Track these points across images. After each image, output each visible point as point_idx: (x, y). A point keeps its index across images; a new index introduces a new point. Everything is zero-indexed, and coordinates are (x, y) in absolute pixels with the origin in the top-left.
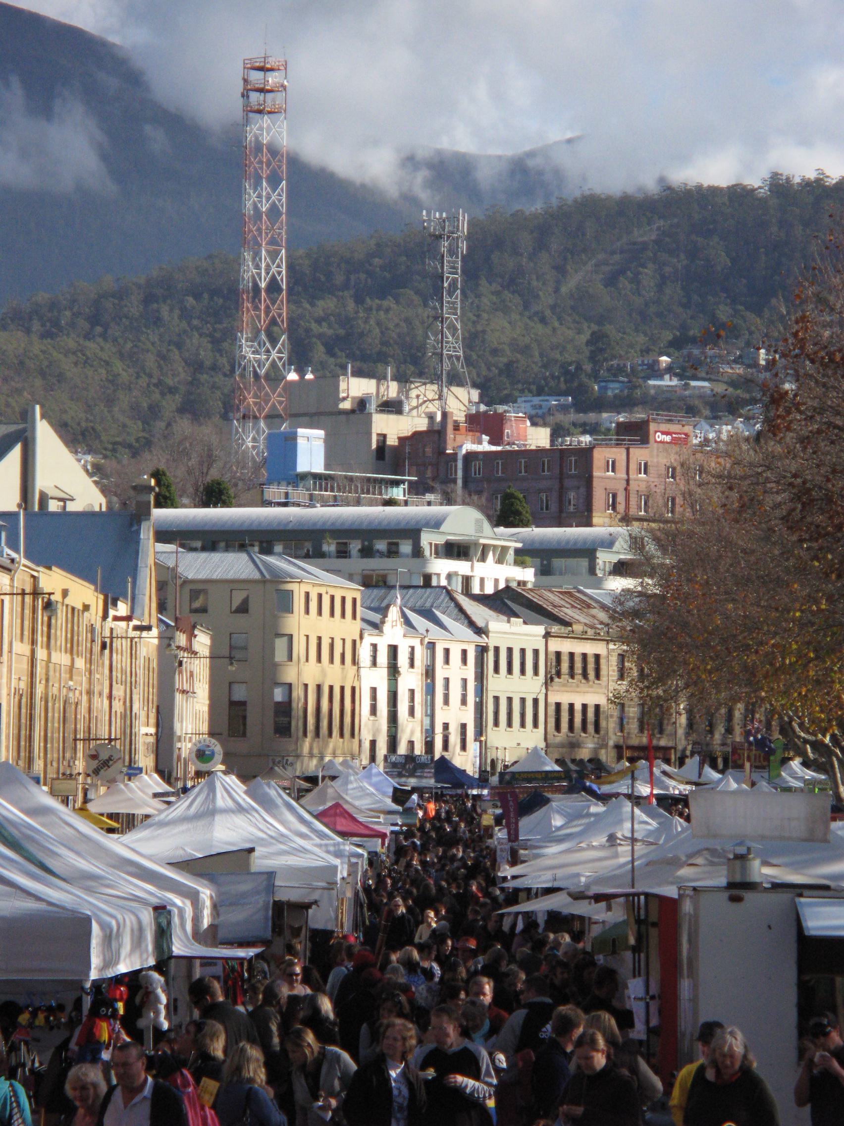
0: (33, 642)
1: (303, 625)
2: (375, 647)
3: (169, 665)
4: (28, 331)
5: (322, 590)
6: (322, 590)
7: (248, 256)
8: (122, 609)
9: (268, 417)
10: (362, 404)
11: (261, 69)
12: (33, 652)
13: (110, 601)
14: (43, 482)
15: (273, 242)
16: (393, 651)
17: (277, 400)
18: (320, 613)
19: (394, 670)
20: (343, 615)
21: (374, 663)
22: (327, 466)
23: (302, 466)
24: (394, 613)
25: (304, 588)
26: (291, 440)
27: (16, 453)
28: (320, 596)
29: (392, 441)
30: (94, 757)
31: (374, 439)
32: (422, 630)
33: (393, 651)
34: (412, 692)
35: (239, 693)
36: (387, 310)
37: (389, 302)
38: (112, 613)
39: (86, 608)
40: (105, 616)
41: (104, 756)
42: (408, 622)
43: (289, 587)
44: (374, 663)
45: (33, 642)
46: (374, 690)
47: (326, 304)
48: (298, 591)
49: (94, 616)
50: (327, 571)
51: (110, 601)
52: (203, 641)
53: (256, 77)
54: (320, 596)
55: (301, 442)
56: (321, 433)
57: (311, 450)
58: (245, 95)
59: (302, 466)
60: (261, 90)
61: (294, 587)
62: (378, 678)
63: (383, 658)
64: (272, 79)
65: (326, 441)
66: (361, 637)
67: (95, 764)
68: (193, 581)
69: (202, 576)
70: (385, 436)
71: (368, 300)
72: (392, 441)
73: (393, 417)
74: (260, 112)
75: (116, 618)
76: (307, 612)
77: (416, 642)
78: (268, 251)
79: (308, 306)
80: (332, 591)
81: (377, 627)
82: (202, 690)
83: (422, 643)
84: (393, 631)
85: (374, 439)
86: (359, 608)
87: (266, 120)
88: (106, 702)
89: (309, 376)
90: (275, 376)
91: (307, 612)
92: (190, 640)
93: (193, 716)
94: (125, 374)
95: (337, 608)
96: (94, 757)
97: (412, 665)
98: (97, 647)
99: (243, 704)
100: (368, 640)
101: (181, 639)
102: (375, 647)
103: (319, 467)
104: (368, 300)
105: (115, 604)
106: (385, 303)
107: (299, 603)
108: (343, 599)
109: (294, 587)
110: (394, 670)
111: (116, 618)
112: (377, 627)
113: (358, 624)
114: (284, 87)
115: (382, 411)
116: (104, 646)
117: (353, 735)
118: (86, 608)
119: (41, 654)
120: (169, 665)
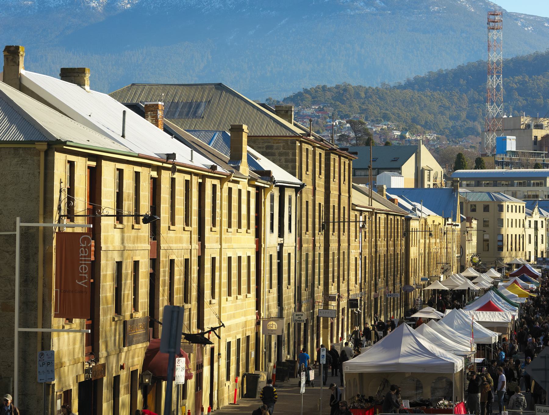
0: (425, 238)
1: (507, 216)
2: (530, 221)
3: (464, 232)
4: (413, 89)
5: (513, 204)
6: (513, 204)
7: (489, 77)
8: (450, 221)
9: (497, 130)
10: (528, 126)
12: (425, 241)
13: (446, 219)
14: (423, 165)
15: (498, 72)
16: (536, 222)
17: (500, 126)
18: (512, 212)
19: (536, 229)
21: (530, 227)
23: (508, 148)
24: (536, 210)
25: (507, 203)
26: (505, 140)
27: (413, 157)
28: (512, 206)
29: (539, 138)
30: (442, 268)
31: (533, 137)
32: (545, 215)
33: (536, 222)
34: (542, 235)
35: (486, 237)
38: (447, 223)
39: (439, 224)
40: (445, 225)
41: (445, 268)
42: (541, 213)
43: (502, 203)
44: (530, 227)
45: (425, 238)
46: (530, 235)
48: (505, 205)
49: (442, 226)
50: (486, 328)
51: (446, 219)
52: (475, 223)
53: (492, 17)
54: (512, 206)
55: (508, 141)
56: (515, 137)
57: (511, 144)
58: (488, 24)
59: (508, 148)
60: (494, 22)
61: (504, 204)
62: (531, 231)
64: (497, 18)
65: (517, 140)
66: (526, 219)
67: (443, 270)
68: (471, 202)
69: (474, 200)
71: (533, 76)
72: (539, 138)
73: (539, 130)
74: (493, 29)
75: (448, 224)
78: (496, 76)
79: (511, 78)
80: (516, 204)
81: (531, 215)
82: (474, 238)
84: (536, 216)
85: (533, 137)
86: (525, 208)
87: (495, 32)
88: (446, 250)
90: (498, 117)
91: (508, 211)
92: (470, 224)
93: (471, 248)
94: (447, 103)
95: (517, 210)
96: (442, 268)
97: (542, 227)
98: (443, 234)
99: (487, 240)
100: (528, 219)
101: (468, 224)
102: (530, 221)
103: (514, 149)
104: (533, 76)
105: (448, 220)
106: (540, 77)
107: (505, 208)
108: (520, 206)
109: (504, 204)
110: (536, 229)
111: (448, 224)
113: (524, 214)
115: (536, 128)
116: (445, 233)
117: (523, 250)
118: (439, 224)
119: (427, 241)
120: (464, 232)
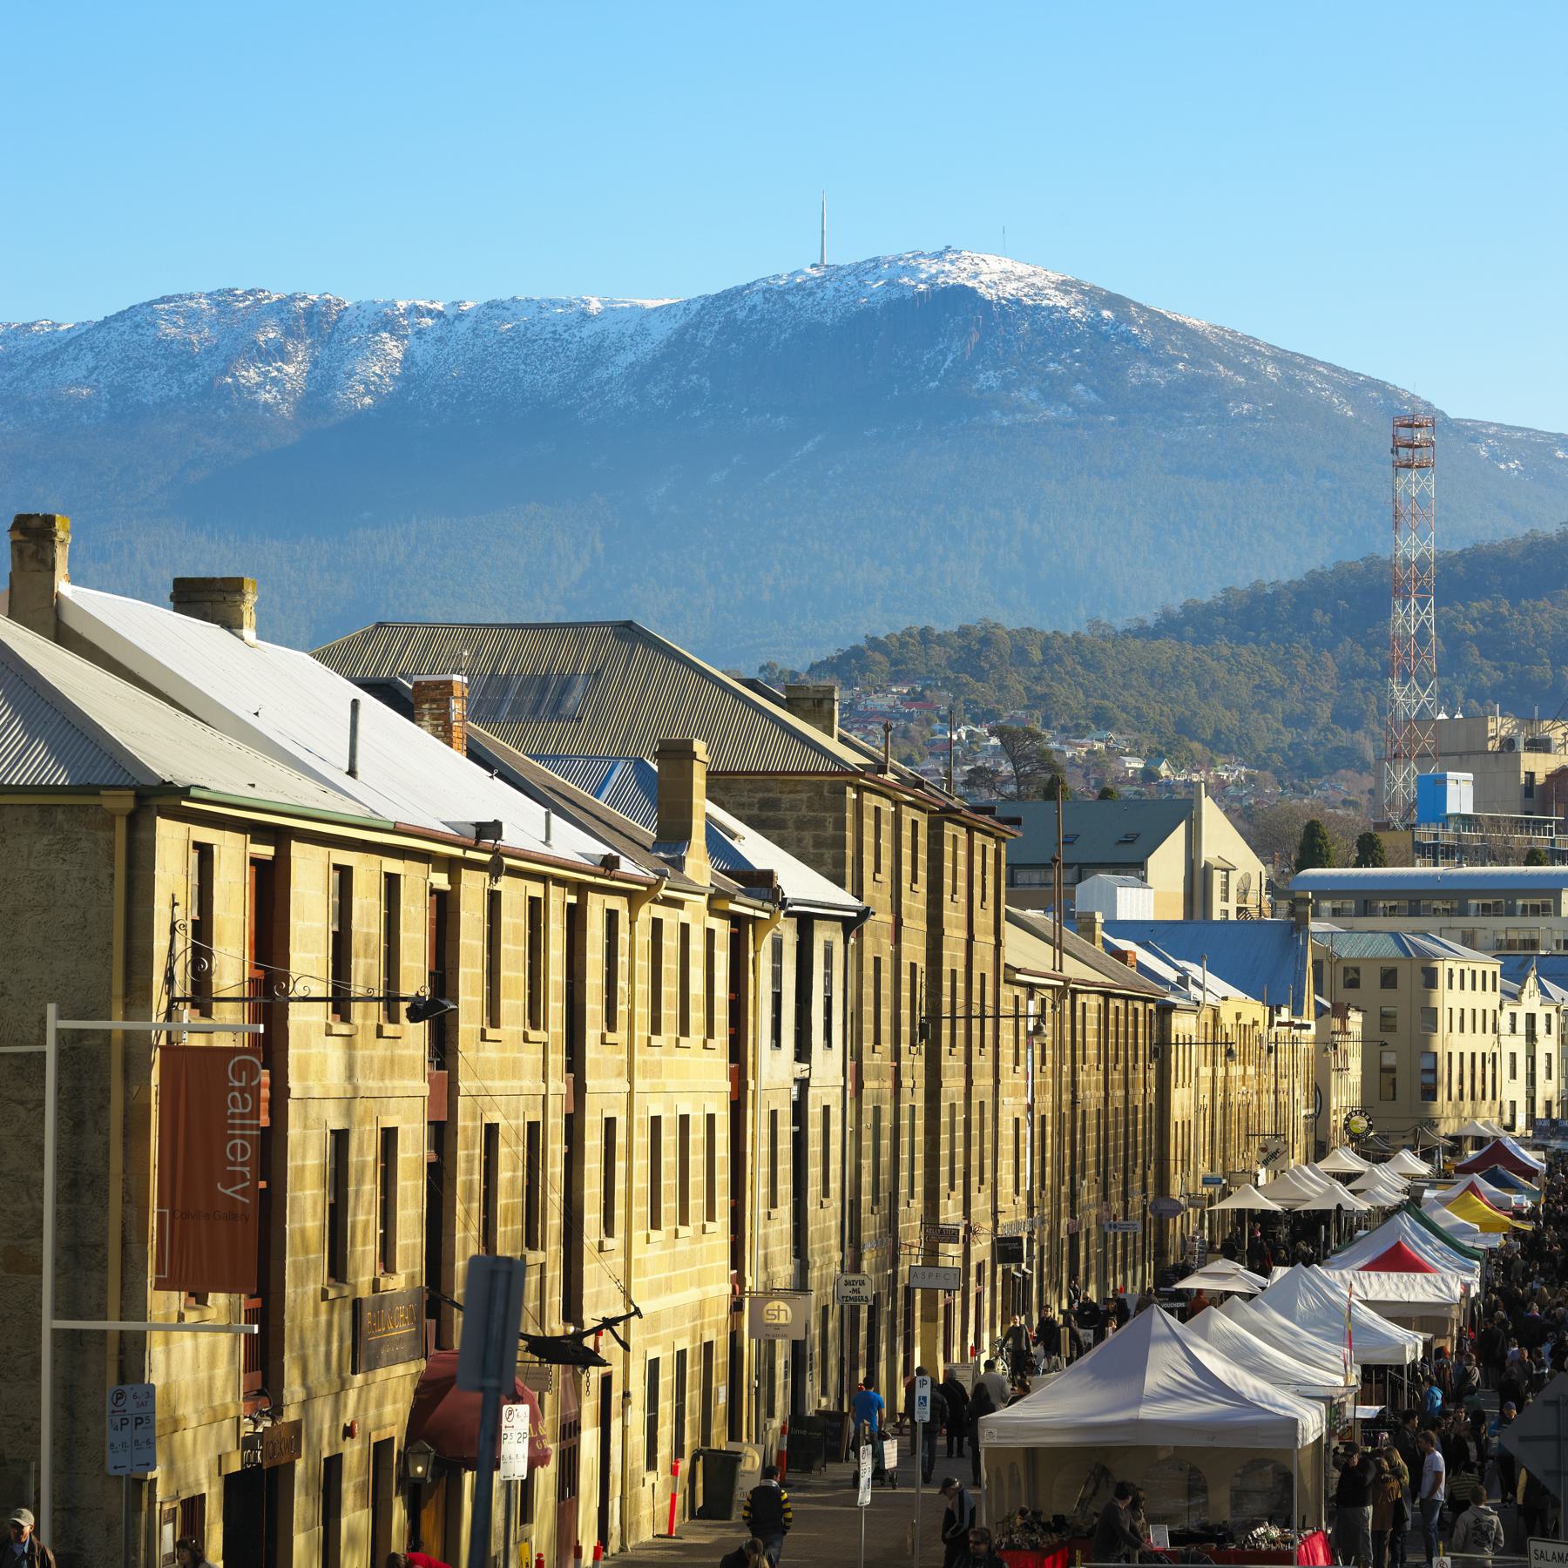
0: (1214, 1063)
1: (1447, 999)
2: (1513, 1015)
3: (1327, 1044)
5: (1464, 966)
6: (1464, 966)
7: (1397, 603)
8: (1285, 1014)
9: (1418, 756)
10: (1509, 744)
11: (1410, 426)
12: (1214, 1071)
13: (1275, 1009)
15: (1422, 590)
16: (1531, 1018)
17: (1427, 742)
19: (1531, 1037)
20: (1484, 989)
21: (1513, 1030)
22: (1476, 806)
23: (1452, 807)
24: (1531, 982)
25: (1448, 964)
28: (1462, 971)
29: (1540, 779)
30: (1263, 1150)
31: (1523, 775)
33: (1531, 1018)
34: (1549, 1055)
35: (1389, 1060)
36: (1541, 612)
37: (1543, 603)
38: (1277, 1019)
39: (1255, 1023)
40: (1270, 1026)
41: (1272, 1149)
42: (1544, 992)
43: (1435, 965)
44: (1513, 1030)
45: (1214, 1063)
46: (1513, 1055)
47: (1478, 607)
48: (1442, 968)
49: (1262, 1028)
50: (1388, 1319)
51: (1275, 1009)
52: (1355, 1020)
53: (1404, 433)
54: (1462, 971)
55: (1451, 786)
56: (1470, 776)
57: (1460, 795)
58: (1395, 451)
59: (1452, 807)
60: (1410, 446)
61: (1439, 965)
62: (1518, 1044)
63: (1521, 1026)
64: (1419, 435)
65: (1476, 784)
66: (1501, 1008)
67: (1264, 1156)
69: (1354, 955)
70: (1532, 774)
71: (1524, 602)
72: (1540, 779)
74: (1409, 466)
75: (1280, 1024)
76: (1451, 987)
77: (1552, 1010)
79: (1461, 607)
80: (1473, 966)
81: (1516, 997)
82: (1355, 1064)
83: (1557, 1010)
84: (1531, 1001)
85: (1523, 775)
86: (1498, 978)
87: (1413, 475)
88: (1272, 1097)
89: (1459, 716)
90: (1423, 718)
91: (1451, 987)
92: (1344, 1024)
93: (1346, 1092)
95: (1478, 982)
97: (1549, 1032)
98: (1264, 1053)
99: (1392, 1070)
100: (1508, 1009)
101: (1336, 1024)
102: (1513, 1015)
103: (1468, 809)
105: (1279, 1012)
106: (1541, 605)
107: (1442, 978)
108: (1484, 973)
109: (1439, 965)
110: (1531, 1037)
111: (1280, 1024)
112: (1516, 997)
114: (1433, 443)
115: (1529, 750)
116: (1270, 1050)
117: (1494, 1098)
118: (1255, 1023)
119: (1221, 1072)
120: (1327, 1044)
